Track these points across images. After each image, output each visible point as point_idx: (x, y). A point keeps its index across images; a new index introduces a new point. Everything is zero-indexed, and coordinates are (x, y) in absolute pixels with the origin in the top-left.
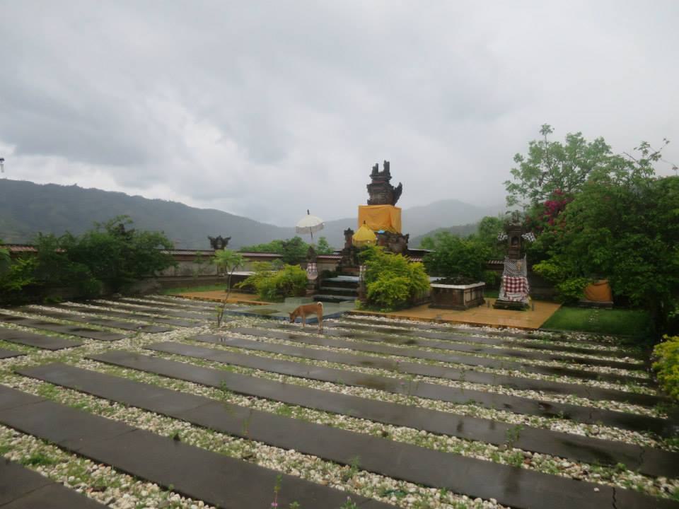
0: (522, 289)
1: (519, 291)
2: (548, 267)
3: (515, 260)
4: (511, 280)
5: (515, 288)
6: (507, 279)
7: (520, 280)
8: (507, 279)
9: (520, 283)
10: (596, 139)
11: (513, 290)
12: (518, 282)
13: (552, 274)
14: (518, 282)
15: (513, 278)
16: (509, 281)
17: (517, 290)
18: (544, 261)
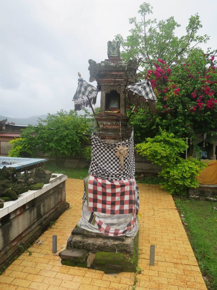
0: (126, 207)
1: (122, 211)
2: (158, 148)
3: (112, 142)
4: (104, 186)
5: (113, 204)
6: (95, 184)
7: (123, 186)
8: (95, 184)
9: (123, 194)
10: (175, 29)
11: (108, 207)
12: (118, 190)
13: (162, 157)
14: (118, 190)
15: (108, 182)
16: (100, 189)
17: (117, 208)
18: (149, 139)
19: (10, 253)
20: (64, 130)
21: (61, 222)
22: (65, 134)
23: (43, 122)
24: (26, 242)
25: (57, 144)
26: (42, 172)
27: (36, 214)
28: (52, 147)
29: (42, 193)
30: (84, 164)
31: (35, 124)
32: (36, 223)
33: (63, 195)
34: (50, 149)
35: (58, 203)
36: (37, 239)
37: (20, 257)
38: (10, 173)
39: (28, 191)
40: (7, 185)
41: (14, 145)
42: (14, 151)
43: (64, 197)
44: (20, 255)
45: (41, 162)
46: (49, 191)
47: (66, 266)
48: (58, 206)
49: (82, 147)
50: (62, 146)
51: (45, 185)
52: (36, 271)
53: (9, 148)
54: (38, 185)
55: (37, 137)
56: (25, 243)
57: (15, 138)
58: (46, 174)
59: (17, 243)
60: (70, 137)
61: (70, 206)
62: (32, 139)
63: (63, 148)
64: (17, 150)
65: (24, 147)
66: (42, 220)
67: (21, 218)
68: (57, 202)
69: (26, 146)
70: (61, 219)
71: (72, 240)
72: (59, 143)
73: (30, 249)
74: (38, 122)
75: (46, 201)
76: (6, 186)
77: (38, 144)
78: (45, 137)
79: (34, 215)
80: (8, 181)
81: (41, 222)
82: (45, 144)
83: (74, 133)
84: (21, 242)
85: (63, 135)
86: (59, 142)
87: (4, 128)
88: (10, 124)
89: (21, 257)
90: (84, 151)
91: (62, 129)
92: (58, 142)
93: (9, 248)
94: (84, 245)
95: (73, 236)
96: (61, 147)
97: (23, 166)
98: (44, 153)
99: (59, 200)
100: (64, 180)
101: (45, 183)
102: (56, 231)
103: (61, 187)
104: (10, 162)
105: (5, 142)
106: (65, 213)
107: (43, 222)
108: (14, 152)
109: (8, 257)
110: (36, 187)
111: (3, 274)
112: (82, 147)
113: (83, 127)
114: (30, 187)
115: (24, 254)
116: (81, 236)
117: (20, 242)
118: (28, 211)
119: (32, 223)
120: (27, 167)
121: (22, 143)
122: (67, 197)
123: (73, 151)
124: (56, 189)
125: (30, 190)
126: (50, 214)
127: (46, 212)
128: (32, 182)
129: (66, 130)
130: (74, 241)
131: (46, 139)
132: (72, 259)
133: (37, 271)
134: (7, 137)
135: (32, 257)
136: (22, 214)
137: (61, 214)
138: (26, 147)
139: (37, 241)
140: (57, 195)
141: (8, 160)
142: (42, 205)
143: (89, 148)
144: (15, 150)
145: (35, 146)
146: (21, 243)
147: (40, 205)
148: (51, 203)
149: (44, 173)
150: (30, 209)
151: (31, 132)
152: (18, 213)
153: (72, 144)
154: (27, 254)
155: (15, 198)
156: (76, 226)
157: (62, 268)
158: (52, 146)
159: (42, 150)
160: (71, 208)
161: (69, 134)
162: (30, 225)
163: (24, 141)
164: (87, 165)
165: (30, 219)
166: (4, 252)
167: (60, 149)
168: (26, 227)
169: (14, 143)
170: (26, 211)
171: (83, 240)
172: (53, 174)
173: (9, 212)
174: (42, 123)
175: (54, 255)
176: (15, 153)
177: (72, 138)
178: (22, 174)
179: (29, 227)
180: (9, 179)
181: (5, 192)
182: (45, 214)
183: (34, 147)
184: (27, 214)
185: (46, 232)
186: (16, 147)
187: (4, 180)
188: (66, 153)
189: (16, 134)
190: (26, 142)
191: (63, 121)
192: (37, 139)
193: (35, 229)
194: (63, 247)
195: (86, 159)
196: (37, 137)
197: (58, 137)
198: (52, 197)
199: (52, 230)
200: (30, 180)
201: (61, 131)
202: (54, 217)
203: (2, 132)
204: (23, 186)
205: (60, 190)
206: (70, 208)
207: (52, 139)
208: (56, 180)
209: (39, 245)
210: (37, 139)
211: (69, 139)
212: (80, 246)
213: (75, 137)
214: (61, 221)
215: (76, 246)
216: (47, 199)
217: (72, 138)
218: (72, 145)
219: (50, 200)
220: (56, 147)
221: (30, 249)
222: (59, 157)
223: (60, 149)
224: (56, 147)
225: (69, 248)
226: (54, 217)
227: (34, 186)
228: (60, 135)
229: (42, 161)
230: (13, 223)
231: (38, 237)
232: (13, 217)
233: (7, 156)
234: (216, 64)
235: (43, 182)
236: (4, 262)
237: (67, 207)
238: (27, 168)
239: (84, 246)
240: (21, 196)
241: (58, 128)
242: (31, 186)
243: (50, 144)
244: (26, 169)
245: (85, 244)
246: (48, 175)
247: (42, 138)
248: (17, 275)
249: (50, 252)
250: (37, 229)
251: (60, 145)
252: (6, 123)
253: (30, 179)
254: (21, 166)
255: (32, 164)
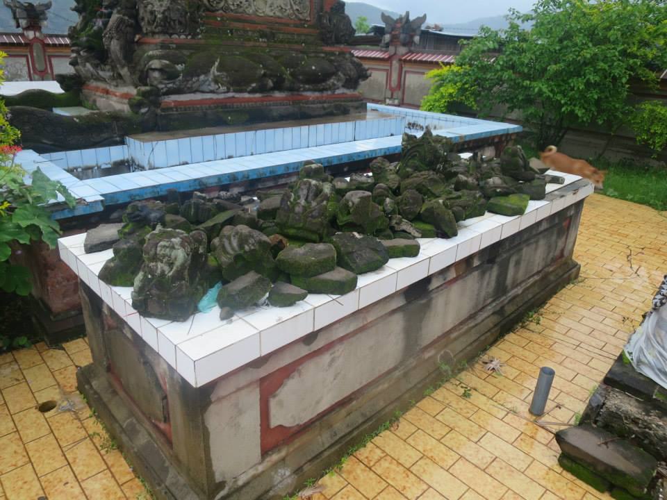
19: (415, 378)
20: (586, 44)
21: (552, 317)
22: (588, 56)
23: (520, 20)
24: (457, 354)
25: (555, 85)
26: (521, 162)
27: (493, 284)
28: (540, 93)
29: (523, 227)
30: (618, 152)
31: (502, 29)
32: (489, 307)
33: (570, 240)
34: (529, 101)
35: (554, 260)
36: (485, 350)
37: (438, 391)
38: (442, 152)
39: (482, 214)
40: (430, 188)
41: (436, 82)
42: (434, 97)
43: (569, 246)
44: (440, 386)
45: (506, 133)
46: (539, 224)
47: (575, 478)
48: (551, 269)
49: (629, 101)
50: (571, 93)
51: (533, 205)
52: (480, 457)
53: (424, 90)
54: (513, 200)
55: (501, 63)
56: (455, 356)
57: (441, 64)
58: (532, 169)
59: (437, 354)
60: (601, 65)
61: (582, 275)
62: (485, 69)
63: (572, 99)
64: (443, 97)
65: (462, 90)
66: (506, 301)
67: (455, 289)
68: (551, 255)
69: (467, 86)
70: (553, 308)
71: (604, 404)
72: (562, 83)
73: (466, 375)
74: (507, 20)
75: (526, 251)
76: (429, 190)
77: (500, 81)
78: (522, 64)
79: (488, 284)
80: (436, 177)
81: (501, 305)
82: (519, 83)
83: (615, 56)
84: (446, 353)
85: (579, 58)
86: (563, 81)
87: (417, 39)
88: (431, 31)
89: (440, 394)
90: (632, 112)
91: (579, 39)
92: (560, 79)
93: (414, 364)
94: (646, 435)
95: (610, 389)
96: (565, 96)
97: (461, 137)
98: (511, 109)
99: (558, 252)
100: (581, 198)
101: (532, 199)
102: (539, 341)
103: (571, 217)
104: (426, 125)
105: (416, 76)
106: (563, 291)
107: (506, 308)
108: (435, 101)
109: (410, 386)
110: (506, 207)
111: (392, 429)
112: (629, 101)
113: (647, 37)
114: (491, 203)
115: (448, 385)
116: (637, 400)
117: (442, 352)
118: (476, 273)
119: (480, 307)
120: (470, 141)
121: (457, 79)
122: (576, 248)
123: (600, 111)
124: (557, 221)
125: (490, 211)
126: (527, 289)
127: (519, 281)
128: (498, 190)
129: (590, 45)
130: (614, 409)
131: (526, 70)
132: (600, 468)
133: (482, 459)
134: (421, 62)
135: (469, 405)
136: (461, 278)
137: (555, 293)
138: (466, 90)
139: (485, 358)
140: (554, 238)
141: (427, 120)
142: (513, 259)
143: (651, 107)
144: (438, 96)
145: (490, 89)
146: (446, 353)
147: (508, 260)
148: (536, 257)
149: (526, 166)
150: (483, 270)
151: (486, 48)
152: (452, 274)
153: (600, 89)
154: (456, 390)
155: (449, 234)
156: (621, 359)
157: (559, 481)
158: (540, 90)
159: (507, 101)
160: (582, 281)
161: (601, 57)
162: (473, 312)
163: (466, 74)
164: (627, 156)
165: (478, 295)
166: (402, 372)
167: (563, 102)
168: (464, 314)
169: (437, 79)
170: (471, 273)
171: (646, 418)
172: (550, 173)
173: (430, 273)
174: (518, 22)
175: (535, 421)
176: (437, 104)
177: (607, 68)
178: (463, 161)
179: (472, 317)
180: (437, 171)
181: (423, 209)
182: (515, 285)
183: (486, 91)
184: (472, 280)
185: (511, 337)
186: (442, 89)
187: (423, 173)
188: (580, 115)
189: (444, 54)
190: (469, 75)
191: (584, 14)
192: (499, 67)
193: (485, 322)
194: (563, 405)
195: (634, 139)
196: (501, 63)
197: (561, 66)
198: (542, 242)
199: (527, 334)
200: (491, 180)
201: (576, 45)
202: (537, 297)
203: (412, 48)
204: (475, 198)
205: (565, 224)
206: (580, 279)
207: (544, 70)
208: (564, 193)
209: (490, 372)
210: (499, 67)
211: (596, 71)
212: (631, 432)
213: (619, 65)
214: (553, 313)
215: (615, 425)
216: (528, 245)
217: (607, 68)
218: (602, 91)
219: (536, 249)
220: (551, 95)
221: (468, 378)
222: (548, 123)
223: (563, 102)
224: (551, 95)
225: (590, 424)
226: (537, 297)
227: (502, 201)
228: (570, 57)
229: (508, 129)
230: (434, 301)
231: (488, 347)
232: (439, 284)
233: (418, 109)
234: (666, 21)
235: (527, 193)
236: (398, 398)
237: (573, 276)
238: (468, 145)
239: (646, 437)
240: (466, 227)
241: (568, 36)
242: (492, 200)
243: (534, 84)
244: (466, 146)
245: (651, 432)
246: (537, 173)
247: (513, 67)
248: (429, 447)
249: (524, 409)
250: (490, 323)
251: (563, 88)
252: (423, 28)
253: (491, 179)
254: (455, 138)
255: (483, 136)
